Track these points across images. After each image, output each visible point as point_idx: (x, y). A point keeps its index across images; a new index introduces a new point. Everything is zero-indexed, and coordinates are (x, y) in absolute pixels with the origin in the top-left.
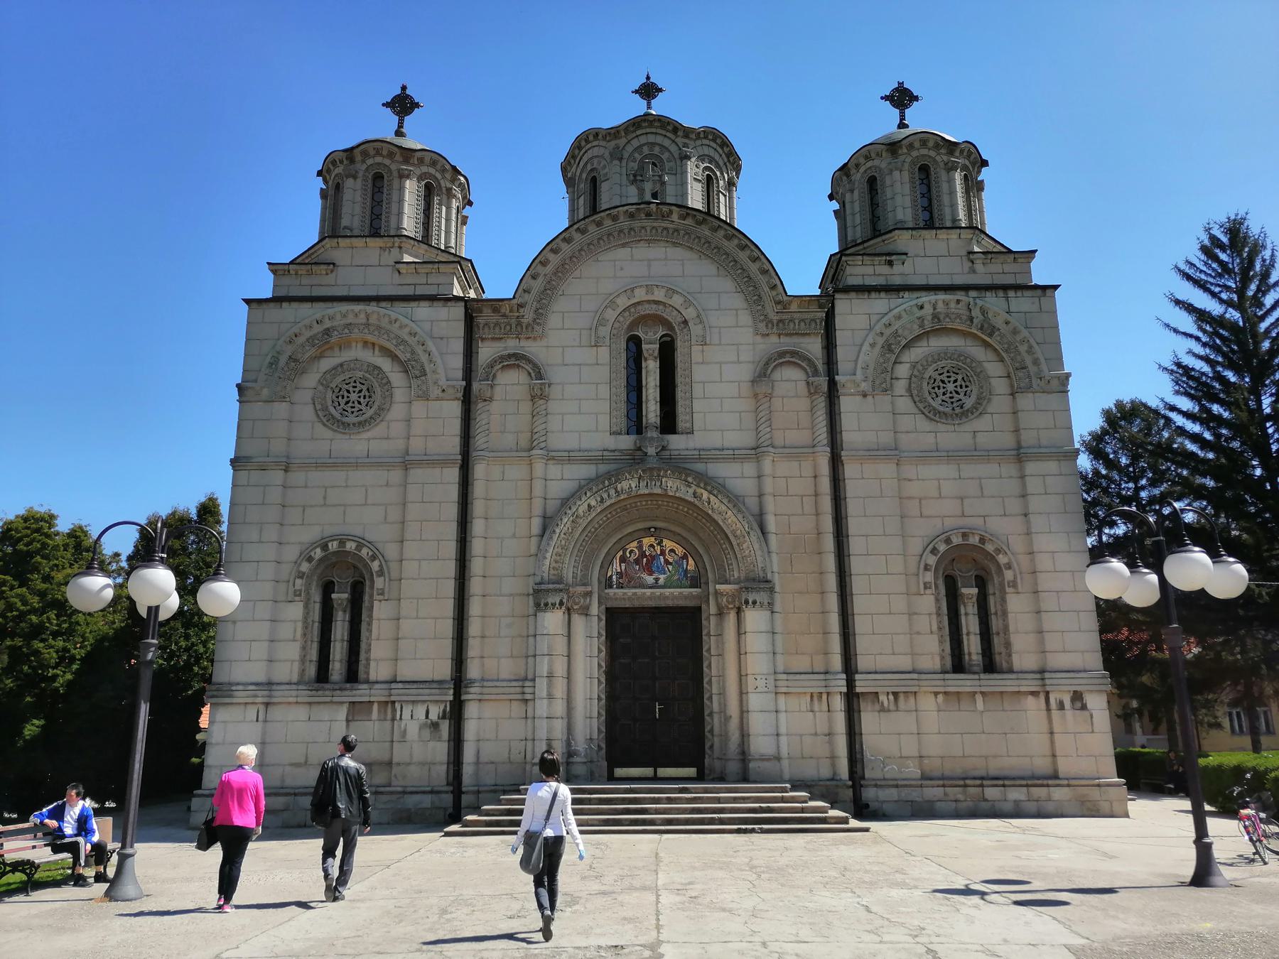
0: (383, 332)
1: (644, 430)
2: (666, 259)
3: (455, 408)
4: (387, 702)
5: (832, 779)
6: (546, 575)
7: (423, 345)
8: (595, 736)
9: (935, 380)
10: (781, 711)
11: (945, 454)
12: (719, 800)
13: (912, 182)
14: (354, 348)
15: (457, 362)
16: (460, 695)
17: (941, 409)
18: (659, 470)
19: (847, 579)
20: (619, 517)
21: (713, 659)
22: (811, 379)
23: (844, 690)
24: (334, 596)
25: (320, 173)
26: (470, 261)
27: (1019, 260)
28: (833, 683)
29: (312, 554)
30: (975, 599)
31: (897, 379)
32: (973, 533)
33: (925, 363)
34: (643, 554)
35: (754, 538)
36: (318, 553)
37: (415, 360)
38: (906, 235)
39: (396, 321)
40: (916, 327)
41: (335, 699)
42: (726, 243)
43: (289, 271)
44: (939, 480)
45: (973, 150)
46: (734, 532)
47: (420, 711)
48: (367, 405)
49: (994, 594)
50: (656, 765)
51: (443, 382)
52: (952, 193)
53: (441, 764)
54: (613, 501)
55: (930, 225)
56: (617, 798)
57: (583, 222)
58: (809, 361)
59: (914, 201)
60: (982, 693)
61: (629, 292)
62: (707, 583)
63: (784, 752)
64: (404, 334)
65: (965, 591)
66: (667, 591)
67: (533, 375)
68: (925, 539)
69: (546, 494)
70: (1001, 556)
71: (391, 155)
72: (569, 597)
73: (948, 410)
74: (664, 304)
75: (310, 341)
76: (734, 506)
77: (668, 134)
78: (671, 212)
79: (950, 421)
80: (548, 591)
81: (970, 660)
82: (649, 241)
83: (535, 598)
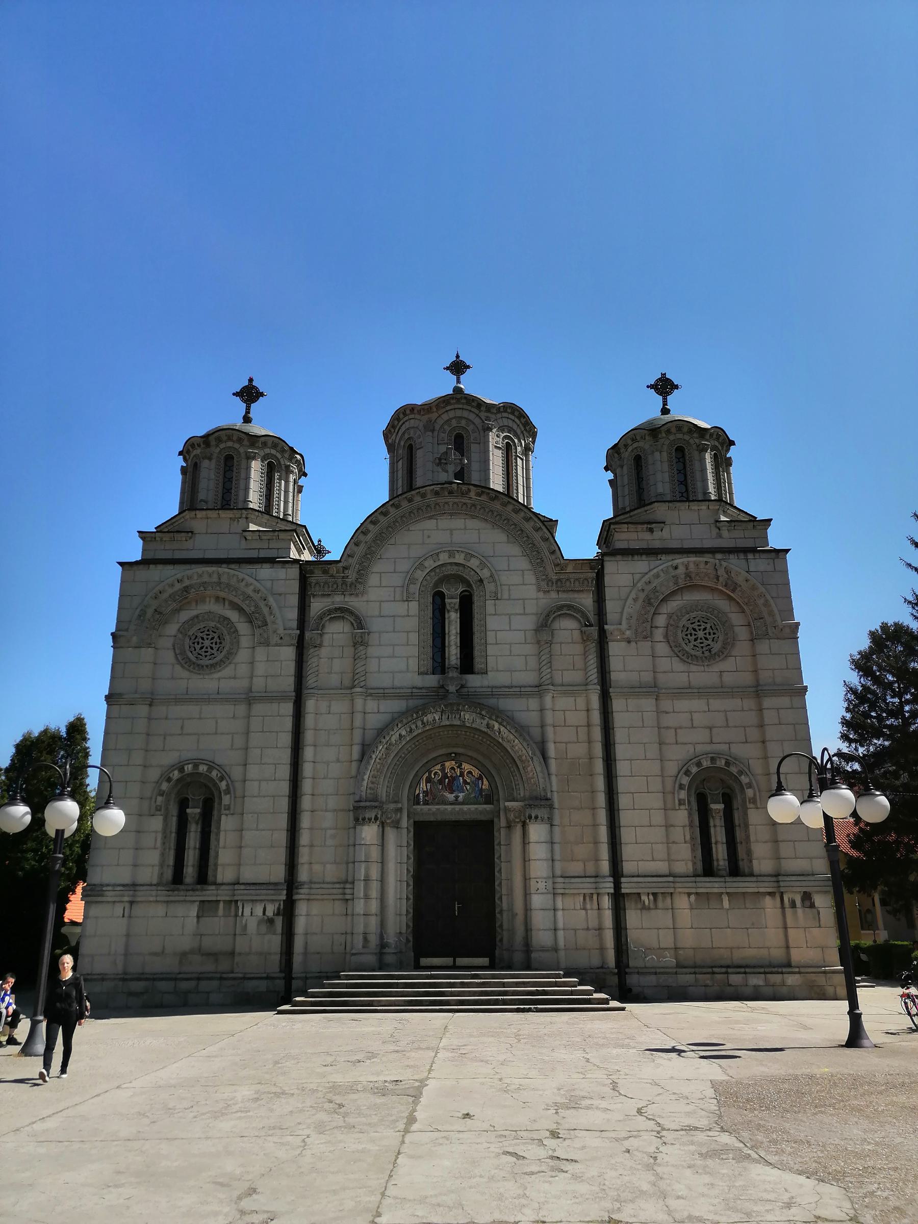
3: (288, 653)
4: (231, 901)
5: (602, 967)
6: (364, 794)
8: (404, 931)
9: (688, 628)
15: (292, 614)
16: (292, 896)
17: (693, 652)
18: (459, 705)
20: (425, 744)
21: (503, 865)
22: (584, 629)
23: (612, 891)
24: (188, 811)
26: (305, 527)
28: (602, 885)
29: (171, 775)
30: (722, 814)
31: (657, 627)
34: (445, 776)
36: (176, 775)
38: (664, 507)
39: (242, 580)
40: (671, 584)
41: (188, 898)
42: (514, 515)
43: (155, 538)
46: (520, 757)
48: (218, 650)
50: (455, 956)
51: (281, 631)
54: (420, 731)
57: (397, 499)
60: (727, 893)
61: (435, 556)
62: (498, 801)
63: (561, 943)
64: (249, 591)
65: (714, 806)
66: (465, 807)
67: (355, 625)
70: (743, 777)
72: (382, 812)
73: (699, 654)
74: (463, 566)
76: (520, 735)
77: (473, 410)
78: (469, 490)
80: (365, 807)
82: (451, 514)
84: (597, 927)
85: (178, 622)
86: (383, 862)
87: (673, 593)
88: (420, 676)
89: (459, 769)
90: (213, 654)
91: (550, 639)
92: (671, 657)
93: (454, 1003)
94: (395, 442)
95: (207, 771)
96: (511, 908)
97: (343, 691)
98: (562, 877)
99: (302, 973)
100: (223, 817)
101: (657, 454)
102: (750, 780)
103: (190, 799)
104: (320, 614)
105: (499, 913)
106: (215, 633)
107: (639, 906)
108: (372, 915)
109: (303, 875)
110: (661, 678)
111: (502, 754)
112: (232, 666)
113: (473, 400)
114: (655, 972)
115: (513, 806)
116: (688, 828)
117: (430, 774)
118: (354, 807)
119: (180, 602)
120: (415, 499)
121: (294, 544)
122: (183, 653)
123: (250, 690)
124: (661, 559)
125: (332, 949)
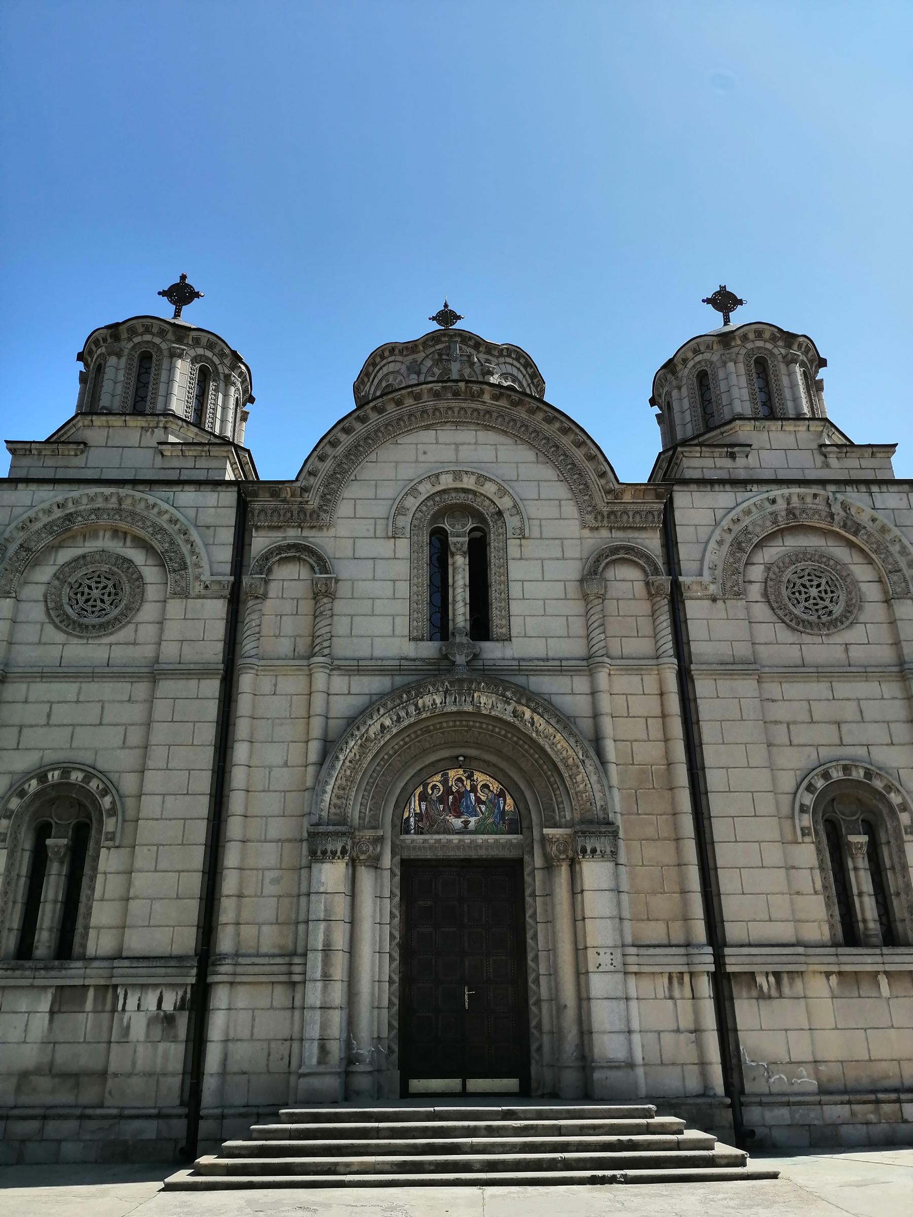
0: (138, 518)
1: (450, 636)
2: (476, 443)
3: (217, 608)
4: (107, 987)
5: (703, 1095)
6: (324, 814)
7: (186, 534)
8: (385, 1034)
9: (794, 584)
10: (631, 999)
11: (814, 670)
12: (559, 1131)
13: (749, 375)
14: (101, 538)
15: (225, 554)
16: (206, 976)
17: (805, 617)
18: (471, 682)
19: (706, 822)
20: (419, 741)
21: (540, 927)
22: (651, 578)
23: (712, 968)
24: (49, 842)
25: (80, 357)
26: (248, 451)
27: (879, 455)
28: (697, 959)
29: (26, 786)
30: (865, 849)
31: (751, 582)
32: (856, 766)
33: (781, 565)
34: (448, 791)
35: (590, 769)
36: (33, 785)
37: (173, 552)
38: (748, 426)
39: (154, 507)
40: (768, 523)
41: (38, 982)
42: (545, 426)
43: (30, 451)
44: (809, 701)
45: (810, 345)
46: (564, 760)
47: (150, 1000)
48: (111, 604)
49: (889, 843)
50: (465, 1075)
51: (206, 577)
52: (793, 386)
53: (173, 1074)
54: (412, 720)
55: (772, 416)
56: (416, 1128)
57: (380, 400)
58: (648, 558)
59: (752, 394)
60: (885, 972)
61: (433, 479)
62: (530, 828)
63: (638, 1057)
64: (163, 521)
65: (853, 839)
66: (480, 838)
67: (317, 568)
68: (798, 772)
69: (327, 711)
70: (892, 795)
71: (162, 333)
72: (353, 843)
73: (814, 618)
74: (475, 493)
75: (48, 527)
76: (564, 728)
78: (482, 392)
79: (816, 631)
80: (328, 834)
81: (866, 928)
82: (457, 424)
83: (310, 844)
84: (692, 1027)
85: (54, 565)
86: (353, 922)
87: (771, 537)
88: (412, 643)
89: (469, 781)
90: (105, 610)
91: (603, 592)
92: (774, 623)
93: (478, 1166)
94: (369, 394)
95: (81, 782)
96: (555, 997)
97: (297, 662)
98: (633, 946)
99: (217, 1107)
100: (103, 851)
101: (731, 365)
102: (904, 798)
103: (54, 825)
104: (266, 553)
105: (534, 1004)
106: (109, 579)
107: (755, 993)
108: (336, 1008)
109: (225, 943)
110: (764, 652)
111: (536, 756)
112: (131, 627)
113: (470, 338)
114: (788, 1100)
115: (554, 835)
116: (818, 871)
117: (425, 788)
118: (309, 833)
119: (59, 535)
120: (406, 402)
121: (232, 466)
122: (59, 607)
123: (157, 660)
124: (751, 491)
125: (268, 1065)
